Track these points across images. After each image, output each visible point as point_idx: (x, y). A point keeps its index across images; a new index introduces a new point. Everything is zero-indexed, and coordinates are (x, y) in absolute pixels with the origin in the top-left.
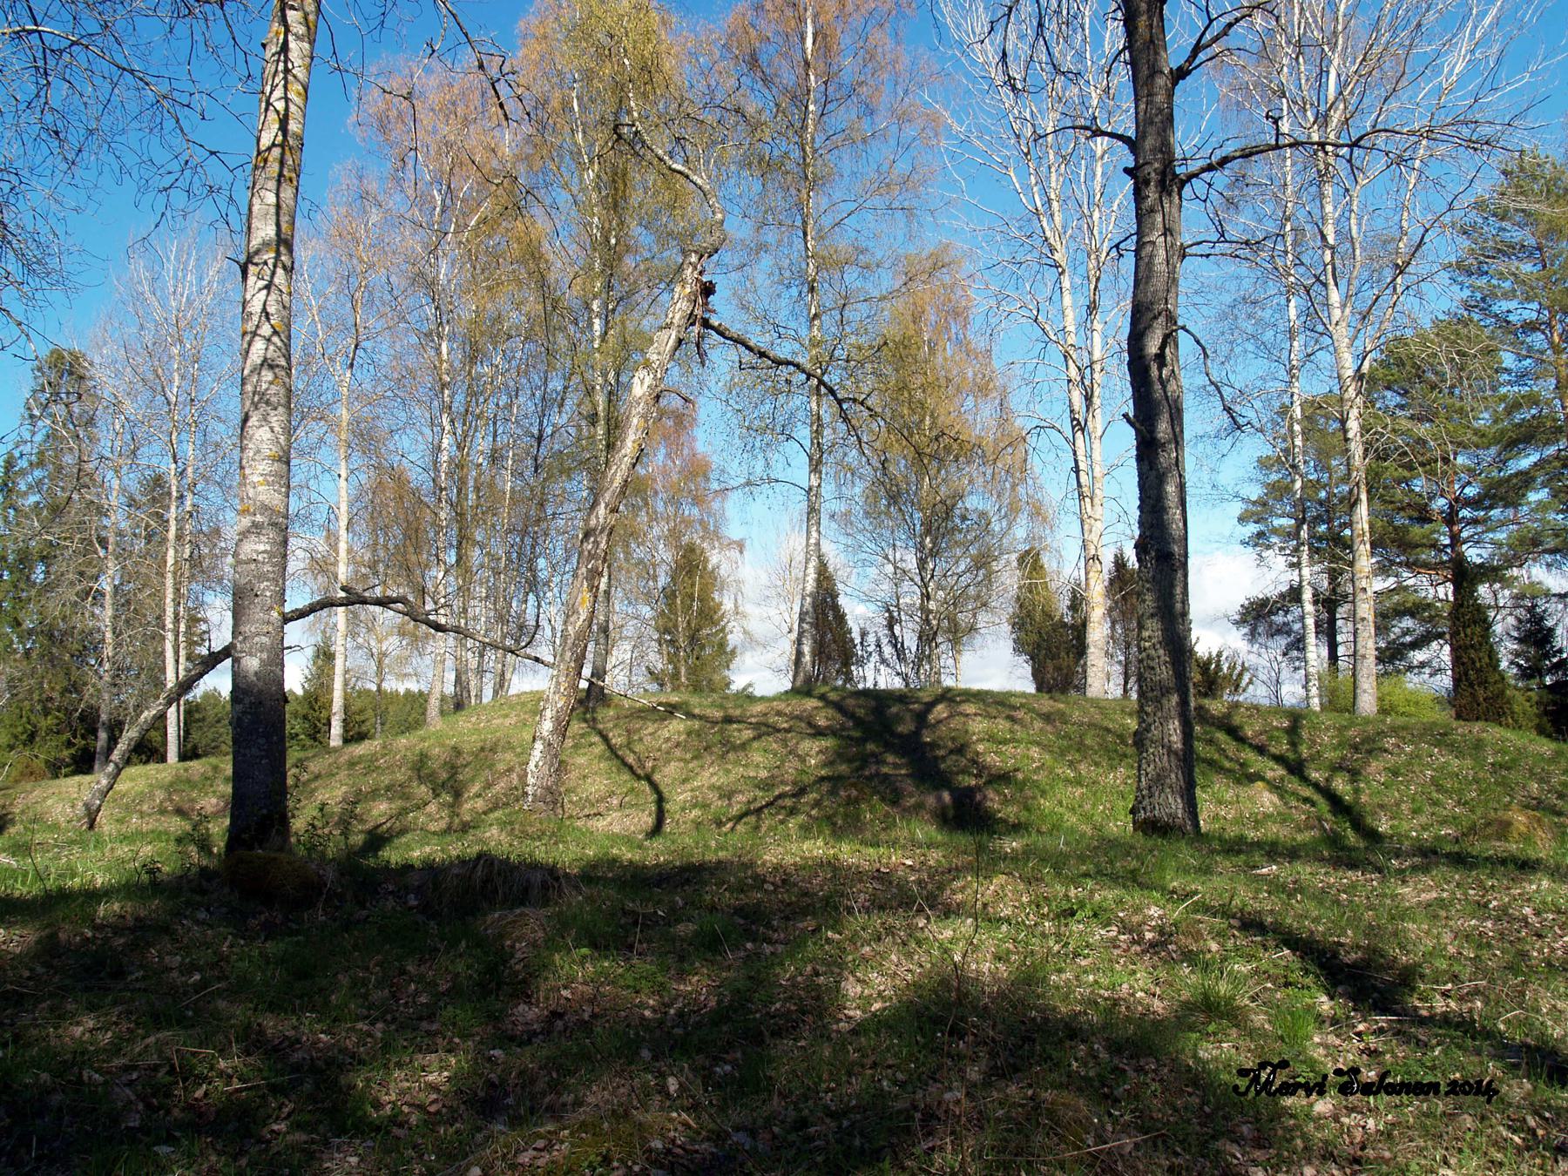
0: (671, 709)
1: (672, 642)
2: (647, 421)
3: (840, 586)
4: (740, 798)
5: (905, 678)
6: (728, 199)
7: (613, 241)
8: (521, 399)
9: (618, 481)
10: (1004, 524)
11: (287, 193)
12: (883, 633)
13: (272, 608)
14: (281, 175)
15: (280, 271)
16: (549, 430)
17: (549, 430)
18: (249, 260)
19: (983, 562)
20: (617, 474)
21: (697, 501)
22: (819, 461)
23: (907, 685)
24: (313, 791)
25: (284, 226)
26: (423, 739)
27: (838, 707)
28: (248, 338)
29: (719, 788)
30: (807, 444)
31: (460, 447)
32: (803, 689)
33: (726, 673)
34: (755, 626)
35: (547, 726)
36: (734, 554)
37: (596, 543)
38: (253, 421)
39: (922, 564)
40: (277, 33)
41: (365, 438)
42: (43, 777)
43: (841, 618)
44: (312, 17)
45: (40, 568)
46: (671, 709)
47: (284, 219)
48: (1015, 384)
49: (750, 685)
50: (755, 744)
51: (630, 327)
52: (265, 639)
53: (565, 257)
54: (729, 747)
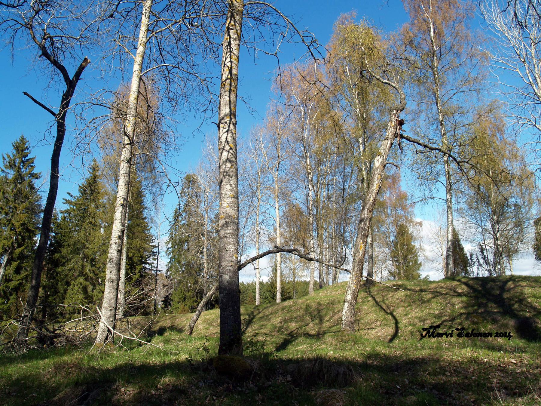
0: (399, 287)
1: (397, 261)
2: (381, 176)
3: (460, 237)
4: (428, 322)
5: (490, 271)
6: (406, 93)
7: (365, 117)
8: (337, 177)
9: (372, 200)
10: (527, 208)
11: (233, 96)
12: (479, 254)
13: (233, 255)
14: (230, 89)
15: (232, 125)
16: (347, 187)
17: (347, 187)
18: (220, 122)
19: (519, 224)
20: (371, 198)
21: (403, 208)
22: (450, 189)
23: (491, 274)
24: (271, 318)
25: (232, 108)
26: (307, 300)
27: (466, 284)
28: (221, 150)
29: (419, 318)
30: (445, 182)
31: (317, 195)
32: (450, 278)
33: (418, 272)
34: (428, 254)
35: (349, 297)
36: (418, 227)
37: (365, 224)
38: (223, 183)
39: (493, 226)
40: (227, 39)
41: (284, 195)
42: (188, 312)
43: (462, 249)
44: (239, 31)
45: (186, 244)
46: (399, 287)
47: (232, 105)
48: (527, 153)
49: (428, 276)
50: (433, 300)
51: (374, 146)
52: (231, 268)
53: (350, 125)
54: (423, 302)
